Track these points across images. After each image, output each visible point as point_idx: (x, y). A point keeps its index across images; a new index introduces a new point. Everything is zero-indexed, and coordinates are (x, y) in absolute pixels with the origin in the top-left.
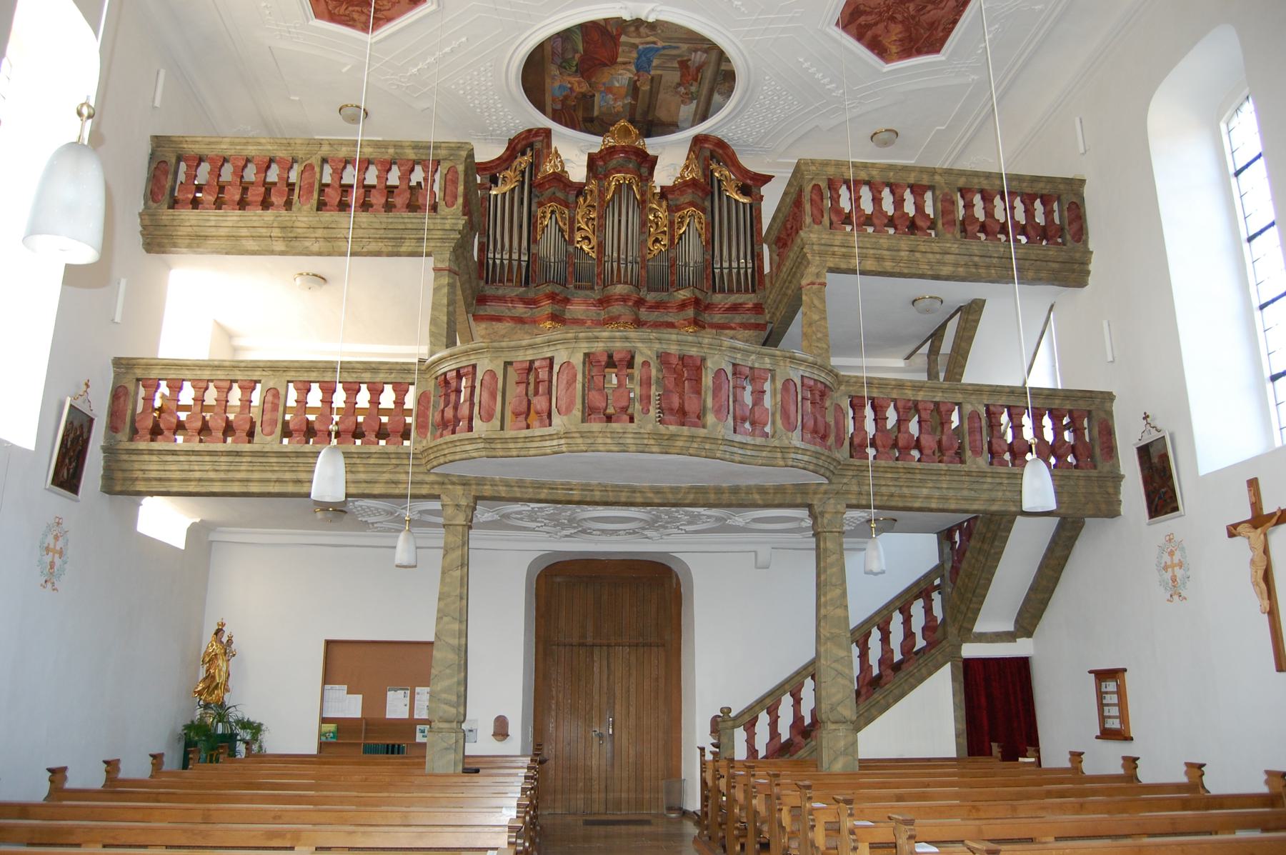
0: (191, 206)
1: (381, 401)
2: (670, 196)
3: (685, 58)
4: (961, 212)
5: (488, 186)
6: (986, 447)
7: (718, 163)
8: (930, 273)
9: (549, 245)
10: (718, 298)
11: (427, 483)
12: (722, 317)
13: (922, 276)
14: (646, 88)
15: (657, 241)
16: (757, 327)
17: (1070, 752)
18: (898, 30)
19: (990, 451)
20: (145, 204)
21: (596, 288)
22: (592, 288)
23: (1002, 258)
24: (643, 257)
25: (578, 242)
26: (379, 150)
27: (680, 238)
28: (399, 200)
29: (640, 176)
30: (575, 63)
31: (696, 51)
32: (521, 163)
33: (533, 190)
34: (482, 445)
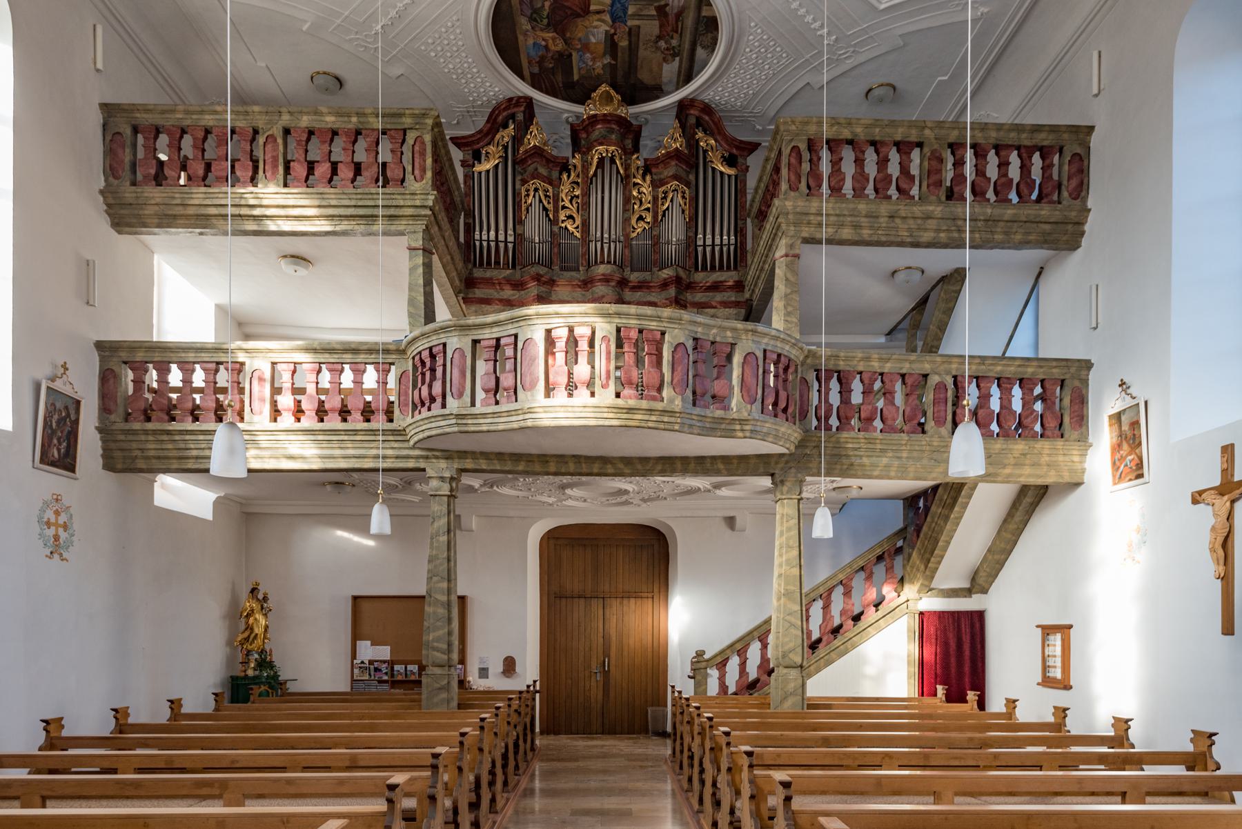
0: (154, 183)
2: (654, 170)
7: (705, 131)
8: (909, 240)
9: (534, 228)
10: (700, 277)
12: (704, 296)
13: (901, 244)
14: (624, 43)
15: (641, 218)
16: (737, 304)
17: (1006, 699)
20: (106, 180)
23: (988, 220)
24: (627, 236)
25: (563, 221)
26: (341, 119)
27: (664, 215)
28: (368, 174)
29: (624, 149)
30: (545, 13)
33: (517, 167)
34: (454, 421)
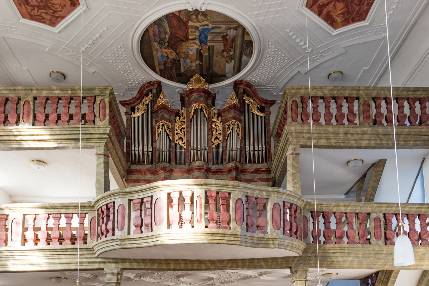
1: (72, 223)
2: (223, 115)
3: (225, 34)
4: (374, 112)
5: (130, 113)
6: (383, 235)
7: (248, 96)
8: (355, 145)
10: (248, 166)
11: (97, 263)
13: (351, 147)
14: (206, 54)
15: (217, 138)
18: (341, 7)
19: (386, 238)
21: (186, 164)
22: (185, 164)
24: (210, 147)
25: (177, 141)
26: (63, 92)
27: (228, 136)
29: (207, 105)
30: (167, 40)
31: (230, 29)
32: (146, 100)
34: (119, 243)
